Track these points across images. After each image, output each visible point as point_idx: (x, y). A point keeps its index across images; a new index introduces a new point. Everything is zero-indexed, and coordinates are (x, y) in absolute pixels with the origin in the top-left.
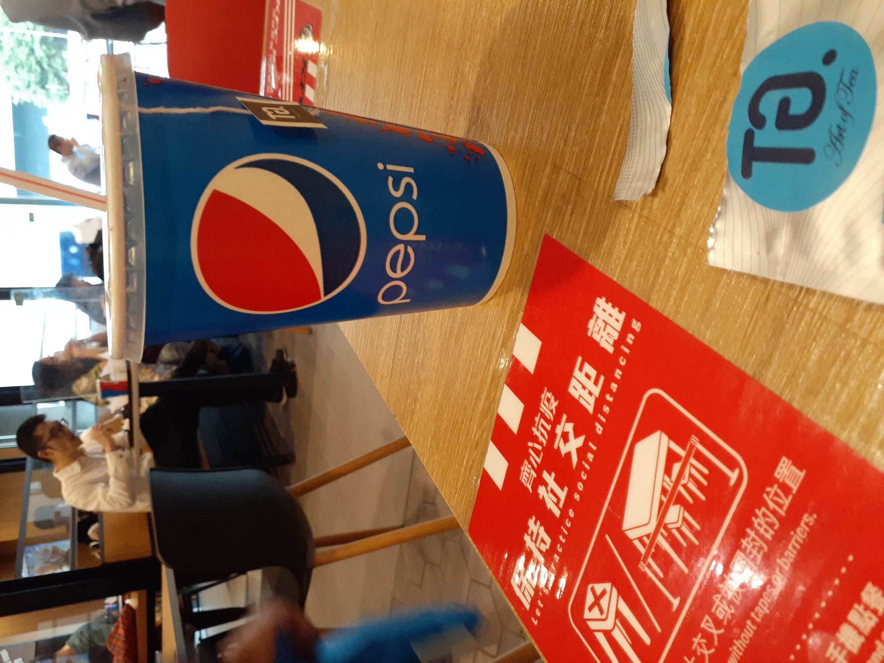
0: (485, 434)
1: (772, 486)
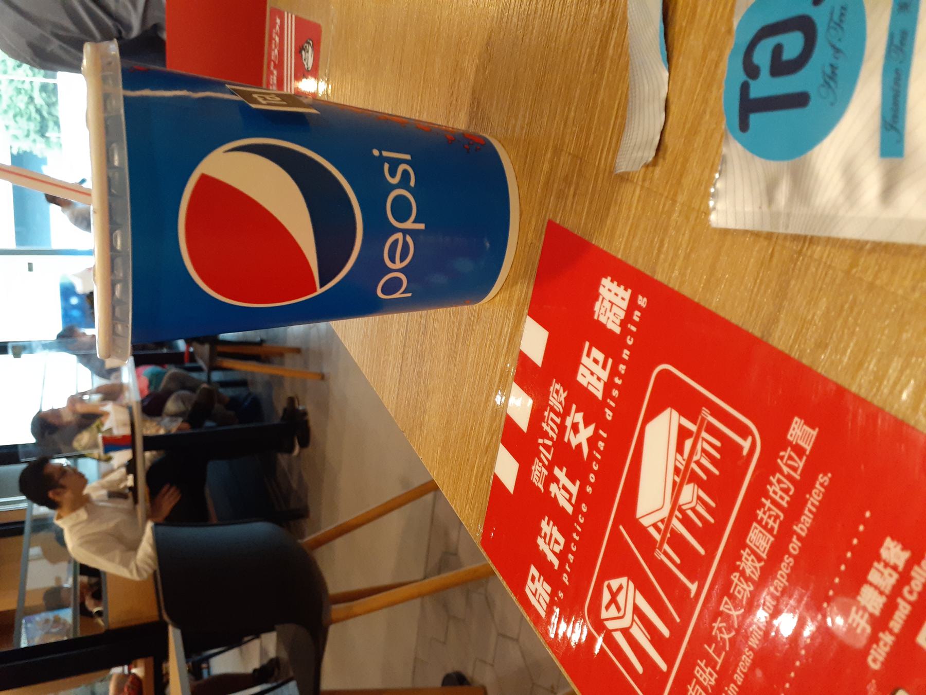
0: (495, 437)
1: (785, 450)
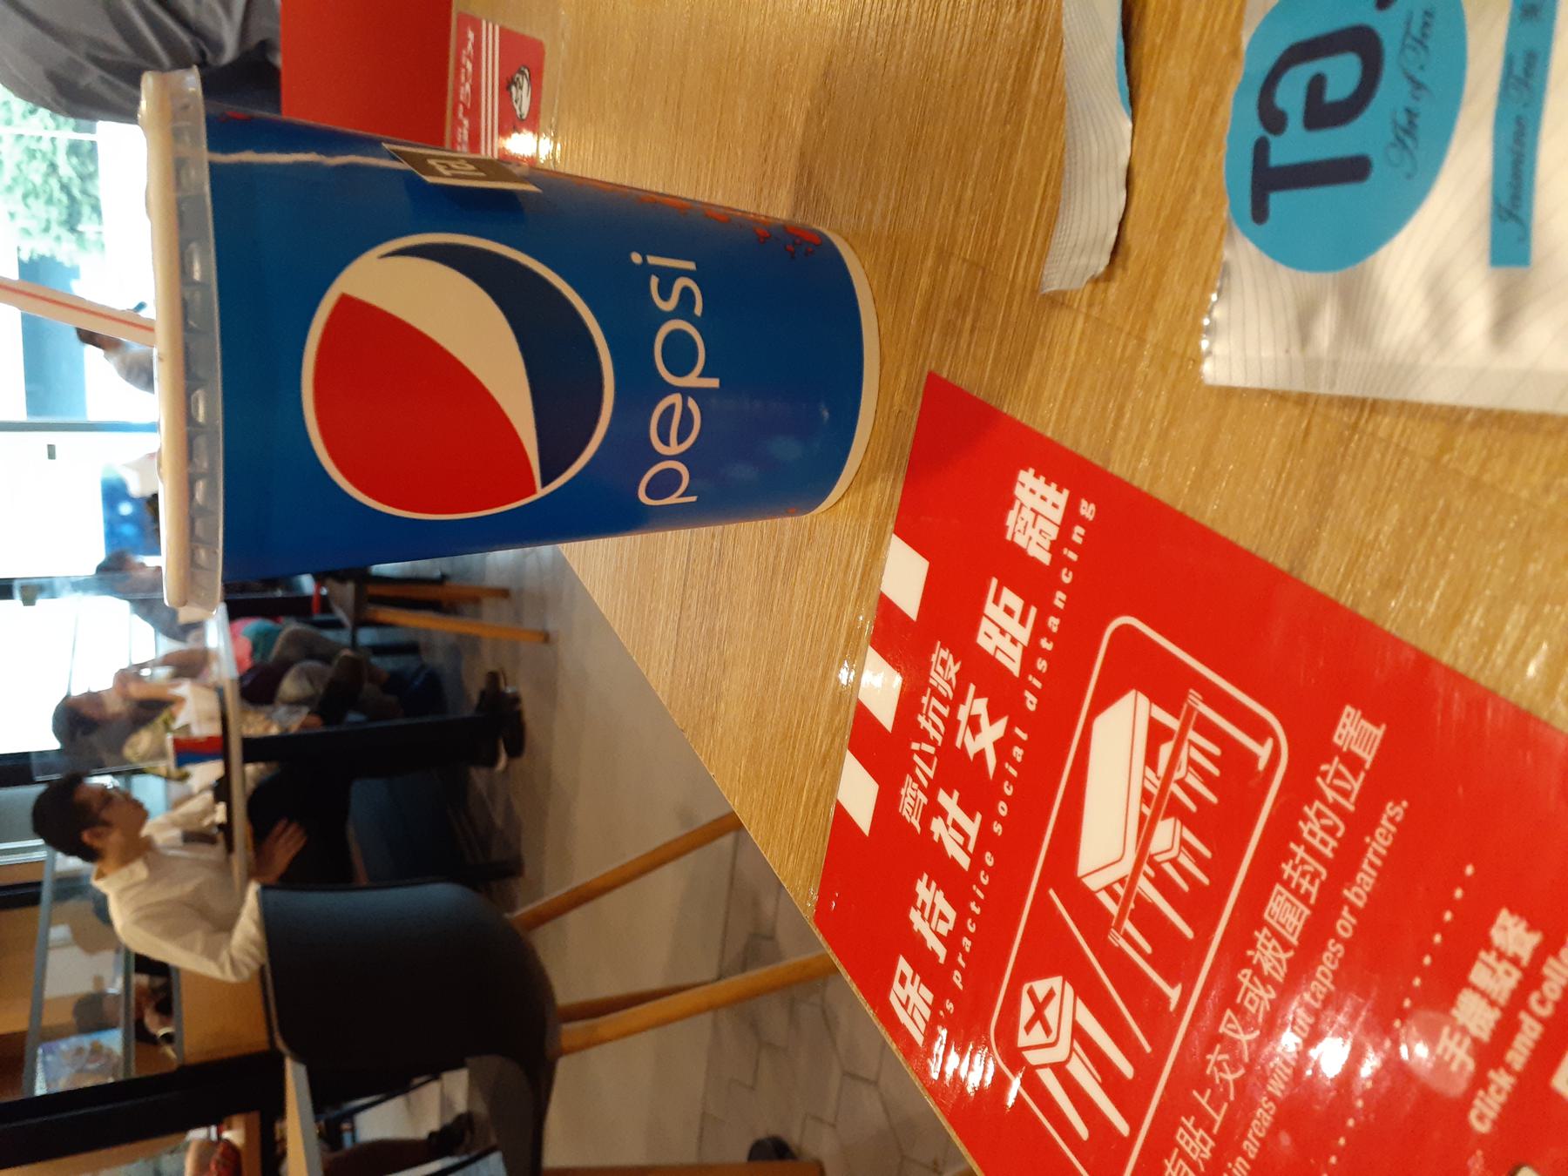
0: (838, 740)
1: (1330, 761)
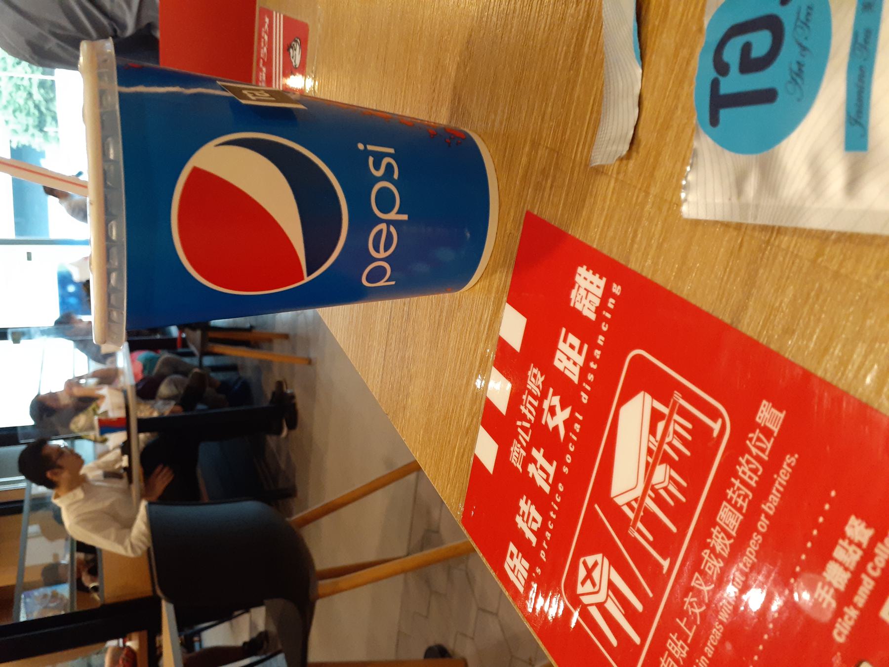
0: (475, 420)
1: (754, 432)
